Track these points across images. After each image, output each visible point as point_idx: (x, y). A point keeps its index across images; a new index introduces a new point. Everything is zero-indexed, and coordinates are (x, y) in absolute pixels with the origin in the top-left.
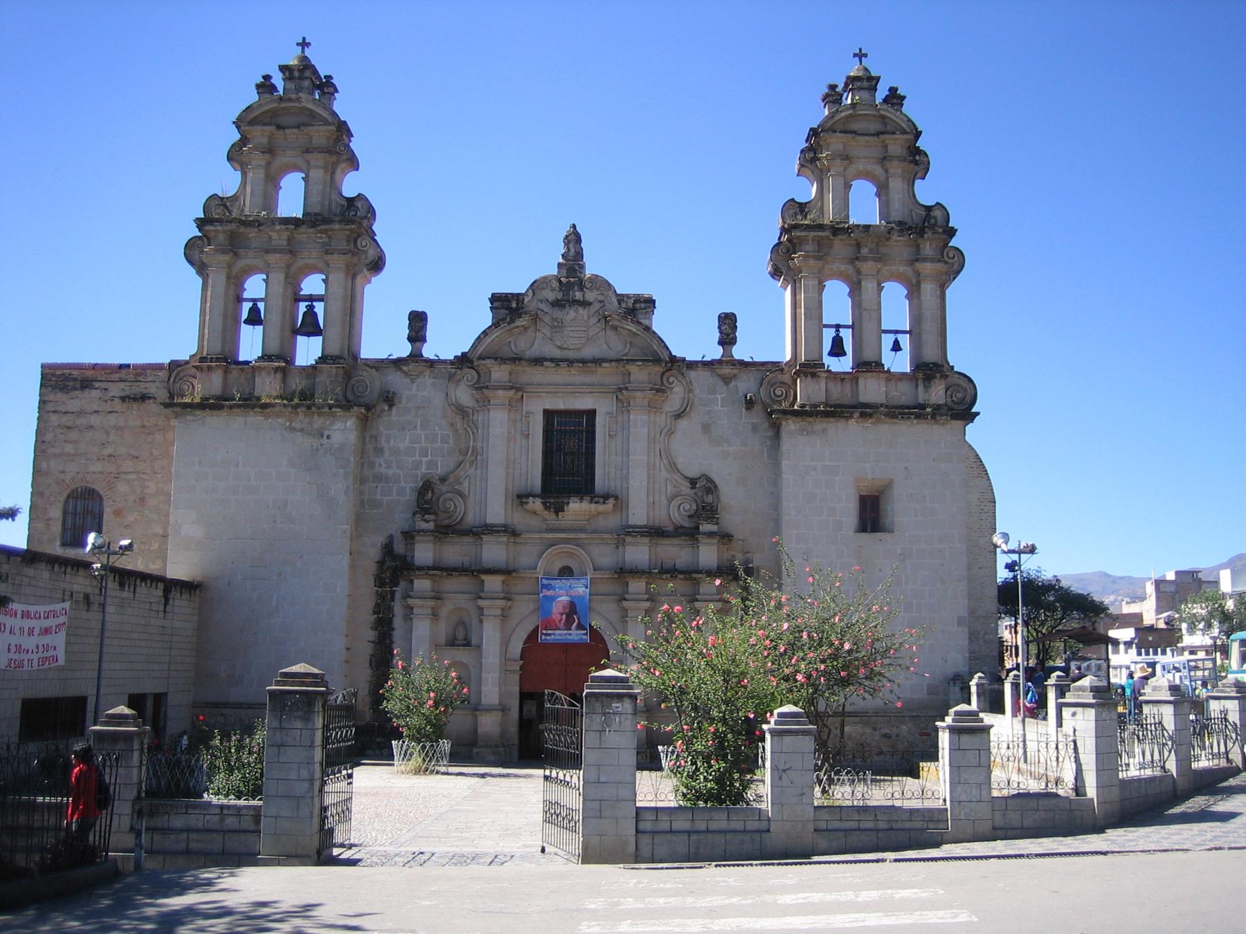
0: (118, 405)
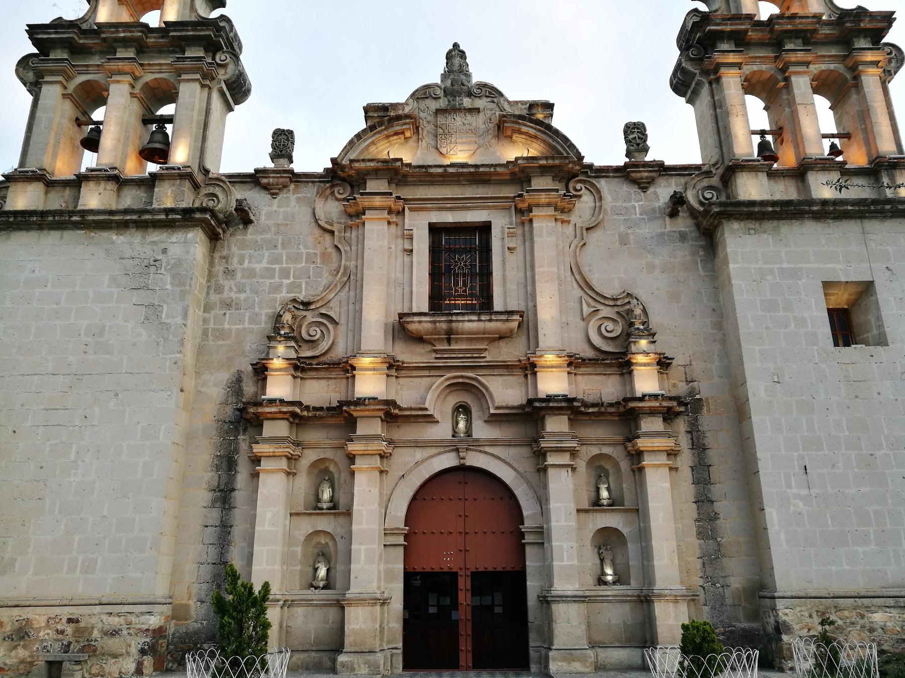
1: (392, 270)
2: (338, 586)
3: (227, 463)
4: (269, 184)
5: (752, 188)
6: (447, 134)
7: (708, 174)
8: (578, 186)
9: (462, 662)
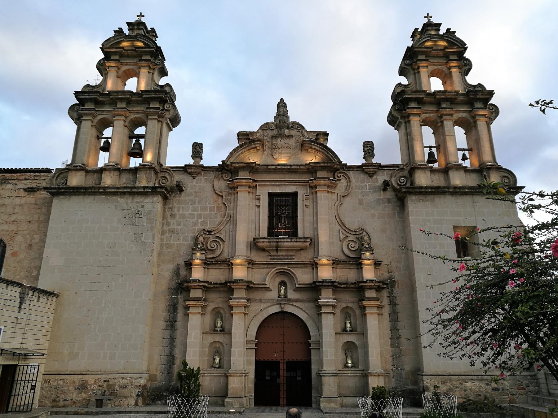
0: (22, 193)
1: (251, 215)
2: (225, 367)
3: (173, 308)
4: (192, 172)
5: (422, 179)
6: (277, 148)
7: (402, 169)
8: (339, 175)
9: (281, 402)
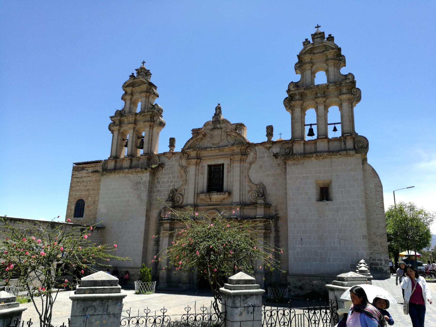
0: (90, 174)
